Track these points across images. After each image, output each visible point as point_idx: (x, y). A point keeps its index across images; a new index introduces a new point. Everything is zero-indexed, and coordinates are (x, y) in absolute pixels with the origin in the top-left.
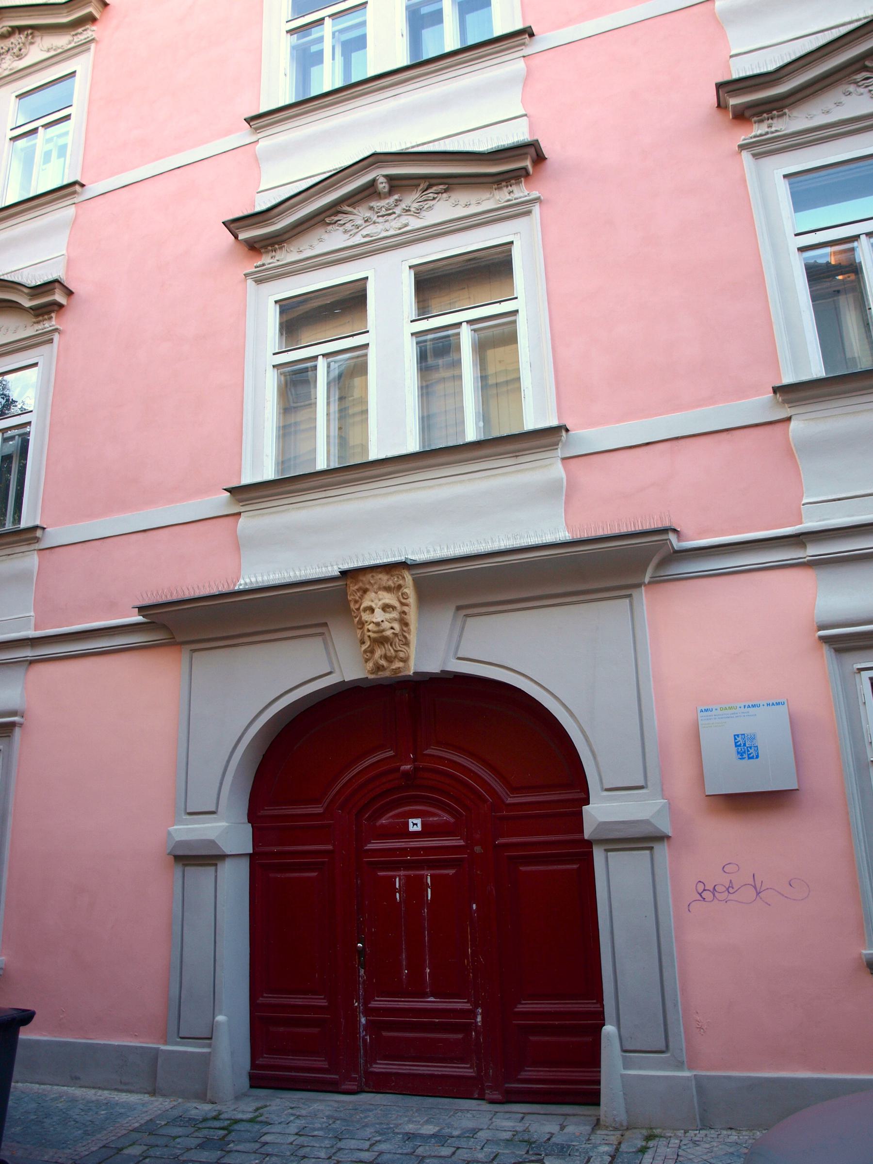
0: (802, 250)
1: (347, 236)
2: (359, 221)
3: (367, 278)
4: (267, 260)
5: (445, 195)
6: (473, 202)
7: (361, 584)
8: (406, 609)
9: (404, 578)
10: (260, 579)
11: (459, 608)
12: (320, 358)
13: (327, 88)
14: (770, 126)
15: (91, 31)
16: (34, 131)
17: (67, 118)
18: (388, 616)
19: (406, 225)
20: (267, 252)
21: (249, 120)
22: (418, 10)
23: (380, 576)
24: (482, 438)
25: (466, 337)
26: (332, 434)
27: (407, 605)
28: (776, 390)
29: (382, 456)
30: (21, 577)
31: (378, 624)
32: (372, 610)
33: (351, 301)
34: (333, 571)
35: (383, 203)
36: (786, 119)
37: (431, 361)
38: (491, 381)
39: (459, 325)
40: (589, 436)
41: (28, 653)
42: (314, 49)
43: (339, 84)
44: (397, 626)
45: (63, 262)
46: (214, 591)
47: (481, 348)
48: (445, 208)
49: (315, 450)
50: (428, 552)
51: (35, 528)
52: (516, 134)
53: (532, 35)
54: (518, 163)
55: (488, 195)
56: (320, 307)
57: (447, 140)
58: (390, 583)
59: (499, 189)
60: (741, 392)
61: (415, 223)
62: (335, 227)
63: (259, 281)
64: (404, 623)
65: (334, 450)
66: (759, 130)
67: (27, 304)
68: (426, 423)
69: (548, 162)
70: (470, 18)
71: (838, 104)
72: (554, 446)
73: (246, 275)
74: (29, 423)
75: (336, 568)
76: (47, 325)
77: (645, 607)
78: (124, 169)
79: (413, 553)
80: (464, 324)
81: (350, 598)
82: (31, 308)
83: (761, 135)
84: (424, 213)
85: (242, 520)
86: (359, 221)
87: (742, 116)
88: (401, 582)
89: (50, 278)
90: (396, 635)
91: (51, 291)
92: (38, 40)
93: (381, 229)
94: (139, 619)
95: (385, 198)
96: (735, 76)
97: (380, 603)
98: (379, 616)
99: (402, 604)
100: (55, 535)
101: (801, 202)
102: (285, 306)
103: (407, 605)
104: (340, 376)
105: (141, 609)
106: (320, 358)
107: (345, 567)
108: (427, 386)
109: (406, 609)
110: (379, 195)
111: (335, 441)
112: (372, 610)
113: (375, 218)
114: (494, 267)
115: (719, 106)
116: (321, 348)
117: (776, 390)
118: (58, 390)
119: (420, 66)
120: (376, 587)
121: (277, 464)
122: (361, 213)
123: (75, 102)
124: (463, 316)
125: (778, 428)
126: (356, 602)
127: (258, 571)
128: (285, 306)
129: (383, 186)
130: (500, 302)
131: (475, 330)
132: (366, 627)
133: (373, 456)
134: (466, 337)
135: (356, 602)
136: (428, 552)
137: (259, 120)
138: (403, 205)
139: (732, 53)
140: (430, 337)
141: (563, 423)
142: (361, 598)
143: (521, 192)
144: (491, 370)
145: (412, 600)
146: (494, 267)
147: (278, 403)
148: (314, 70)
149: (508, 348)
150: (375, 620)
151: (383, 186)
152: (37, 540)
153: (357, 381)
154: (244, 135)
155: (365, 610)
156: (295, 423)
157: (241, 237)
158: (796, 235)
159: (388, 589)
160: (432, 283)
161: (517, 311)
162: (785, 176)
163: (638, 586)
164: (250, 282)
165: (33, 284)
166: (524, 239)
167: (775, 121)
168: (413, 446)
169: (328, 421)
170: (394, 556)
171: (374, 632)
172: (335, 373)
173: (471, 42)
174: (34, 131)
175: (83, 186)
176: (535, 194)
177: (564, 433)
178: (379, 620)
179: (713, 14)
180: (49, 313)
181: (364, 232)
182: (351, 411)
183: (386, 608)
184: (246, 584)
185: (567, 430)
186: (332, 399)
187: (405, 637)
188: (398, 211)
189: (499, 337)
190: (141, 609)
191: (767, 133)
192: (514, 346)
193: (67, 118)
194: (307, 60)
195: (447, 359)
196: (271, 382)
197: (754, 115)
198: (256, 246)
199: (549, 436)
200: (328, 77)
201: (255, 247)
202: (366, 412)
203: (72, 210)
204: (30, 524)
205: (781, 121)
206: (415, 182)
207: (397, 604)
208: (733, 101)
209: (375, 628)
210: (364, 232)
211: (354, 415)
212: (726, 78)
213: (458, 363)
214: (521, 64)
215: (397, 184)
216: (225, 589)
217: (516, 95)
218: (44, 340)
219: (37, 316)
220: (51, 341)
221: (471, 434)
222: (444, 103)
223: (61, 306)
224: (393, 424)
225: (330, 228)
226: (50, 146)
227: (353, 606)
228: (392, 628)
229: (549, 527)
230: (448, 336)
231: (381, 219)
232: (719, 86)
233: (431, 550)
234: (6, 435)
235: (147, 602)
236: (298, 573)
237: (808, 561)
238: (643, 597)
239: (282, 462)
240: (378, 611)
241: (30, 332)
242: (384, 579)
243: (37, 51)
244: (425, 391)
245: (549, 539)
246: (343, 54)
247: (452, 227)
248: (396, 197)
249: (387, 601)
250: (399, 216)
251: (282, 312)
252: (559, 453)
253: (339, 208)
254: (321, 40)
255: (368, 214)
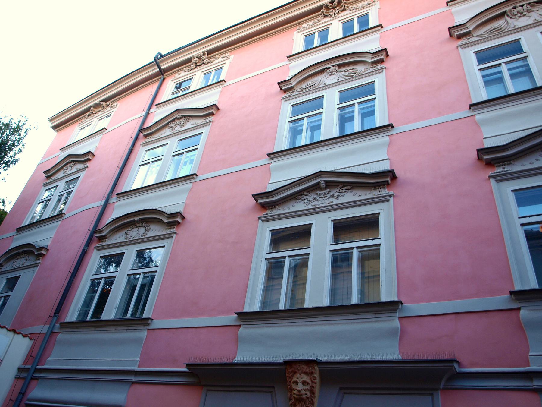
0: (522, 225)
1: (305, 205)
2: (311, 199)
3: (312, 224)
4: (268, 212)
5: (350, 191)
6: (363, 194)
7: (293, 369)
8: (314, 385)
9: (315, 369)
10: (245, 359)
11: (341, 389)
12: (287, 257)
13: (302, 144)
14: (504, 168)
15: (211, 118)
16: (183, 153)
17: (196, 149)
18: (305, 387)
19: (332, 202)
20: (269, 209)
21: (268, 155)
22: (344, 116)
23: (303, 366)
24: (360, 303)
25: (355, 255)
26: (288, 292)
27: (315, 383)
28: (512, 293)
29: (310, 306)
30: (137, 341)
31: (299, 391)
32: (297, 383)
33: (303, 234)
34: (281, 360)
35: (322, 192)
36: (511, 165)
37: (339, 263)
38: (366, 275)
39: (352, 248)
40: (157, 323)
41: (132, 378)
42: (299, 128)
43: (308, 143)
44: (308, 393)
45: (183, 205)
46: (223, 362)
47: (362, 260)
48: (349, 197)
49: (280, 299)
50: (328, 357)
51: (149, 319)
52: (384, 166)
53: (392, 127)
54: (385, 179)
55: (370, 192)
56: (289, 234)
57: (353, 168)
58: (308, 370)
59: (375, 189)
60: (492, 292)
61: (335, 202)
62: (300, 201)
63: (264, 221)
64: (312, 392)
65: (289, 300)
66: (498, 170)
67: (165, 221)
68: (333, 292)
69: (398, 179)
70: (366, 119)
71: (537, 160)
72: (394, 311)
73: (259, 218)
74: (156, 271)
75: (282, 359)
76: (172, 231)
77: (440, 401)
78: (215, 170)
79: (321, 356)
80: (355, 248)
81: (287, 375)
82: (167, 223)
83: (499, 172)
84: (340, 198)
85: (241, 329)
86: (311, 199)
87: (490, 164)
88: (313, 371)
89: (177, 211)
90: (307, 398)
91: (176, 217)
92: (191, 121)
93: (321, 203)
94: (185, 370)
95: (323, 190)
96: (486, 146)
97: (302, 380)
98: (300, 387)
99: (313, 382)
100: (157, 323)
101: (521, 202)
102: (274, 232)
103: (315, 383)
104: (296, 266)
105: (188, 365)
106: (287, 257)
107: (287, 359)
108: (335, 275)
109: (314, 385)
110: (321, 189)
111: (289, 296)
112: (297, 383)
113: (318, 198)
114: (370, 224)
115: (479, 159)
116: (288, 254)
117: (512, 293)
118: (171, 258)
119: (343, 137)
120: (300, 371)
121: (261, 303)
122: (312, 196)
123: (200, 144)
124: (354, 245)
125: (514, 313)
126: (290, 377)
127: (245, 355)
128: (274, 232)
129: (323, 185)
130: (372, 239)
131: (360, 252)
132: (293, 392)
133: (307, 305)
134: (355, 255)
135: (290, 377)
136: (328, 357)
137: (273, 155)
138: (331, 194)
139: (484, 137)
140: (339, 252)
141: (400, 299)
142: (293, 376)
143: (385, 192)
144: (367, 270)
145: (317, 381)
146: (370, 224)
147: (265, 276)
148: (298, 137)
149: (375, 261)
150: (298, 389)
151: (323, 185)
152: (148, 324)
153: (304, 269)
154: (265, 160)
155: (294, 382)
156: (272, 285)
157: (259, 201)
158: (519, 218)
159: (306, 373)
160: (341, 229)
161: (380, 244)
162: (512, 191)
163: (437, 390)
164: (260, 221)
165: (170, 213)
166: (385, 213)
167: (506, 166)
168: (325, 303)
169: (287, 286)
170: (311, 357)
171: (297, 395)
172: (293, 265)
173: (365, 129)
174: (183, 153)
175: (197, 175)
176: (391, 193)
177: (400, 305)
178: (300, 389)
179: (475, 121)
180: (174, 225)
181: (313, 204)
182: (299, 283)
183: (304, 383)
184: (238, 360)
185: (402, 304)
186: (290, 276)
187: (312, 400)
188: (328, 196)
189: (371, 256)
190: (188, 365)
191: (502, 171)
192: (377, 260)
193: (196, 149)
194: (295, 132)
195: (345, 264)
196: (263, 266)
197: (496, 163)
198: (265, 206)
199: (392, 306)
200: (304, 140)
201: (264, 207)
202: (305, 284)
203: (191, 185)
204: (147, 317)
205: (509, 166)
206: (337, 184)
207: (310, 382)
208: (485, 157)
209: (298, 393)
210: (313, 204)
211: (299, 285)
212: (482, 147)
213: (350, 265)
214: (387, 138)
215: (329, 185)
216: (227, 361)
217: (385, 150)
218: (169, 236)
219: (168, 226)
220: (172, 237)
221: (354, 300)
222: (352, 153)
223: (179, 223)
224: (318, 291)
225: (298, 201)
226: (187, 159)
227: (288, 380)
228: (306, 394)
229: (391, 352)
230: (348, 253)
231: (321, 199)
232: (478, 151)
233: (330, 356)
234: (146, 275)
235: (191, 361)
236: (263, 359)
237: (535, 388)
238: (439, 397)
239: (264, 303)
240: (300, 384)
241: (165, 232)
242: (305, 368)
243: (189, 124)
244: (334, 277)
245: (390, 358)
246: (311, 131)
247: (353, 205)
248: (328, 190)
249: (305, 379)
250: (329, 198)
251: (272, 235)
252: (397, 314)
253: (302, 193)
254: (302, 125)
255: (315, 196)
